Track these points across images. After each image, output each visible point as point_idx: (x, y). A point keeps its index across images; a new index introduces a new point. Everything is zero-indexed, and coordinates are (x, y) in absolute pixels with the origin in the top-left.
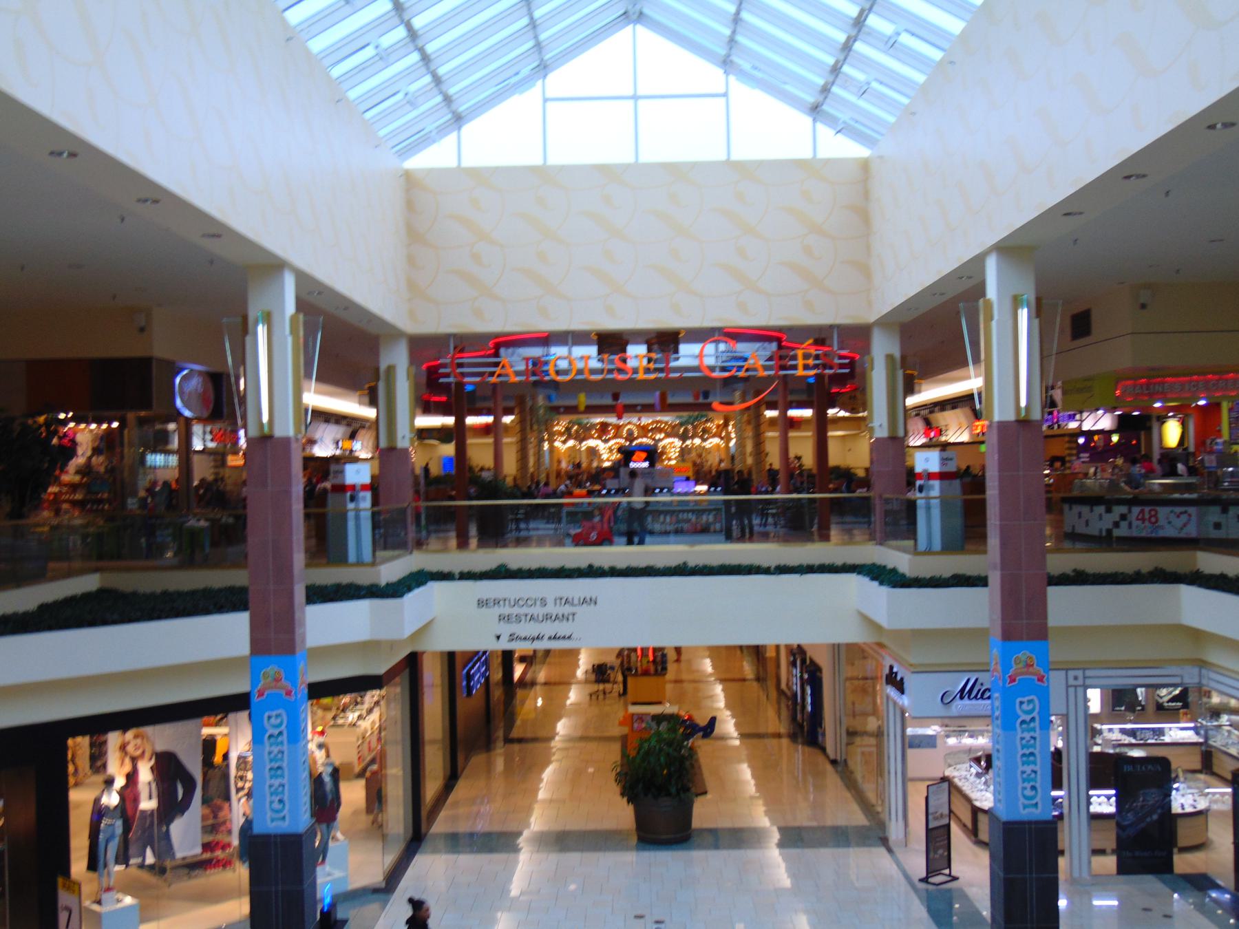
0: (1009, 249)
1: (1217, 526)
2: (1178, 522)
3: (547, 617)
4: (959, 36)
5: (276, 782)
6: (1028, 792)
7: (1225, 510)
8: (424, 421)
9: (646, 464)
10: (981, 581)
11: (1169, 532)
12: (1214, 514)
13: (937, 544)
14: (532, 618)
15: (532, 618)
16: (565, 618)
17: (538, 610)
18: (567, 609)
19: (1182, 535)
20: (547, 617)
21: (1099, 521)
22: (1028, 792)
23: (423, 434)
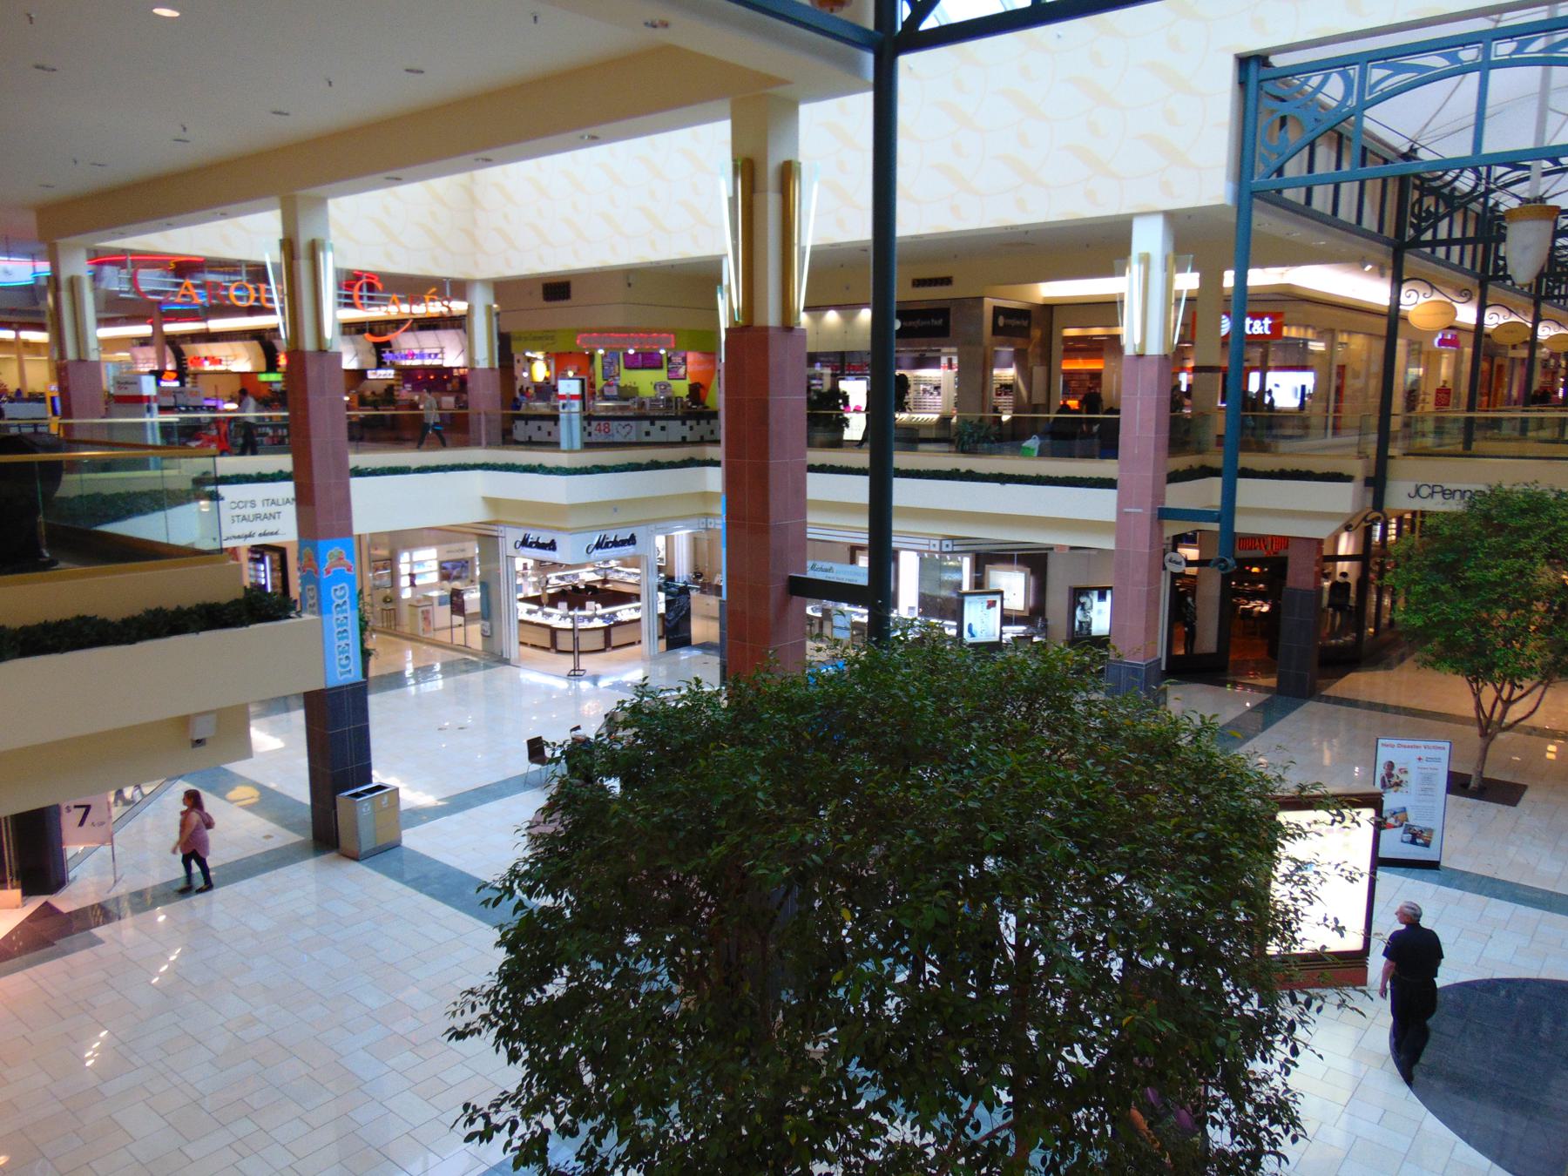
0: (1170, 217)
1: (648, 434)
2: (623, 432)
3: (257, 517)
4: (791, 108)
5: (342, 643)
6: (344, 662)
7: (652, 424)
8: (106, 332)
9: (177, 384)
10: (1349, 479)
11: (618, 438)
12: (646, 425)
13: (577, 445)
14: (244, 518)
15: (244, 518)
16: (272, 516)
17: (249, 511)
18: (273, 509)
19: (627, 440)
20: (257, 517)
21: (619, 431)
22: (344, 662)
23: (110, 345)
